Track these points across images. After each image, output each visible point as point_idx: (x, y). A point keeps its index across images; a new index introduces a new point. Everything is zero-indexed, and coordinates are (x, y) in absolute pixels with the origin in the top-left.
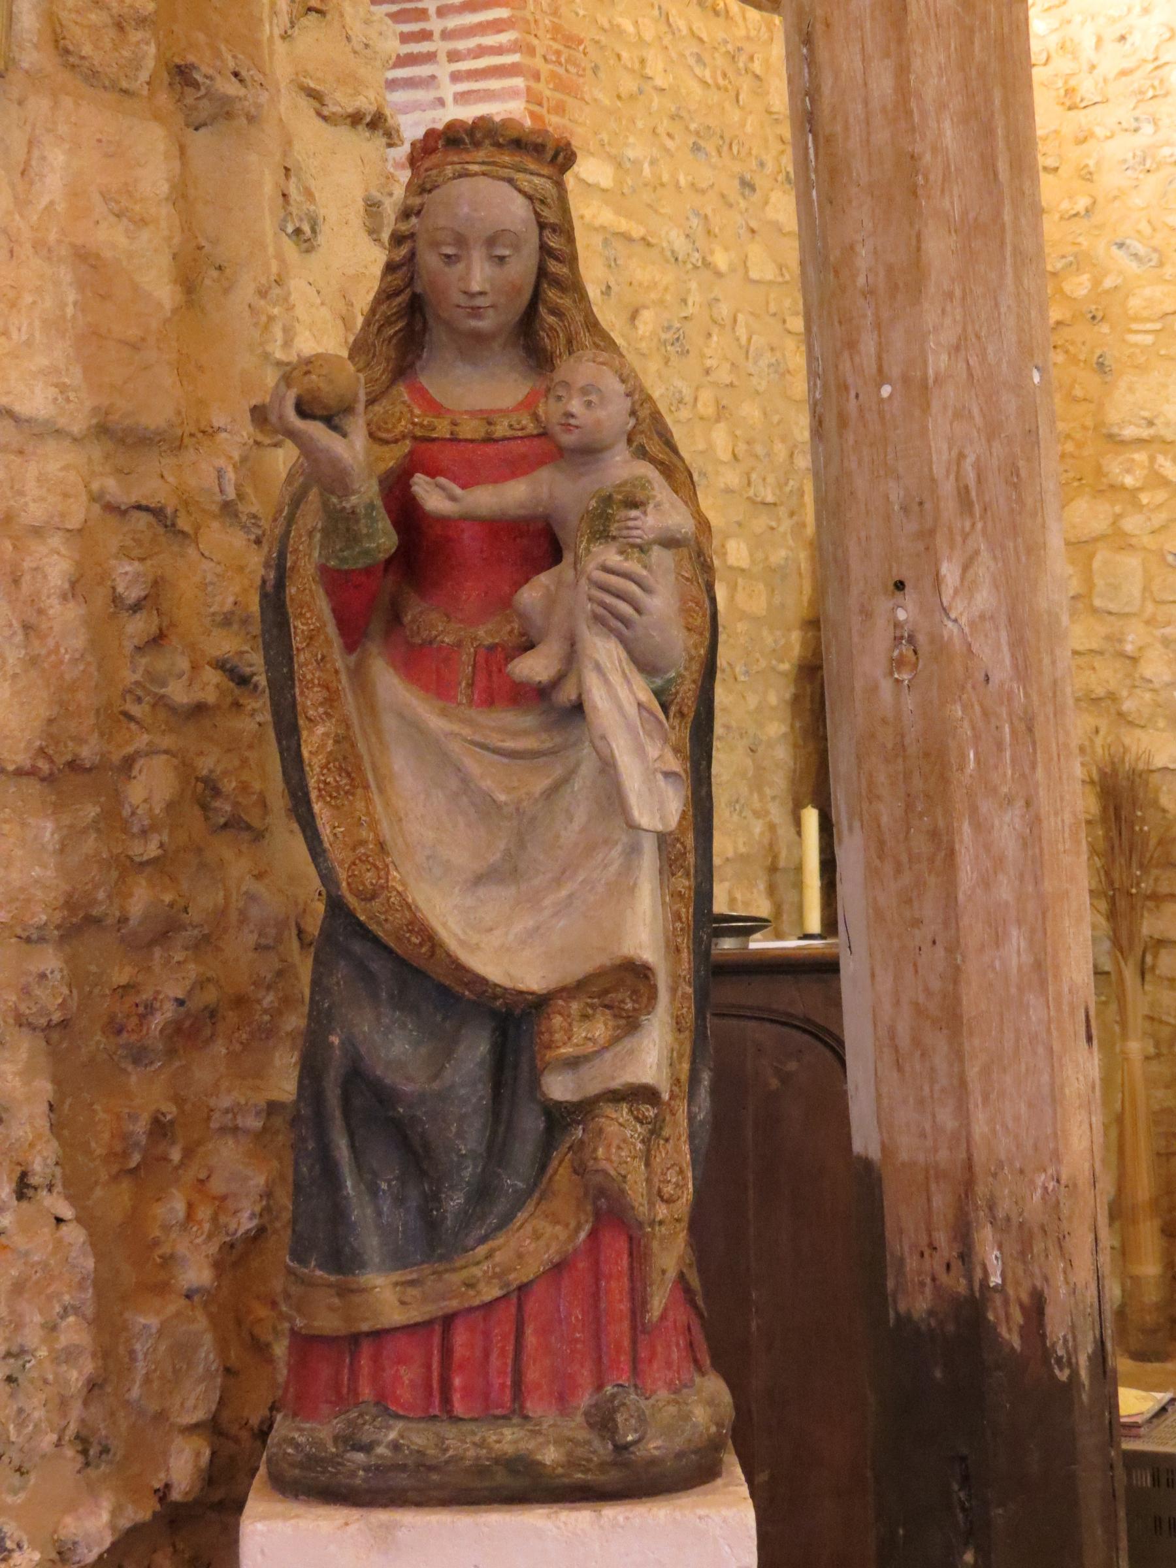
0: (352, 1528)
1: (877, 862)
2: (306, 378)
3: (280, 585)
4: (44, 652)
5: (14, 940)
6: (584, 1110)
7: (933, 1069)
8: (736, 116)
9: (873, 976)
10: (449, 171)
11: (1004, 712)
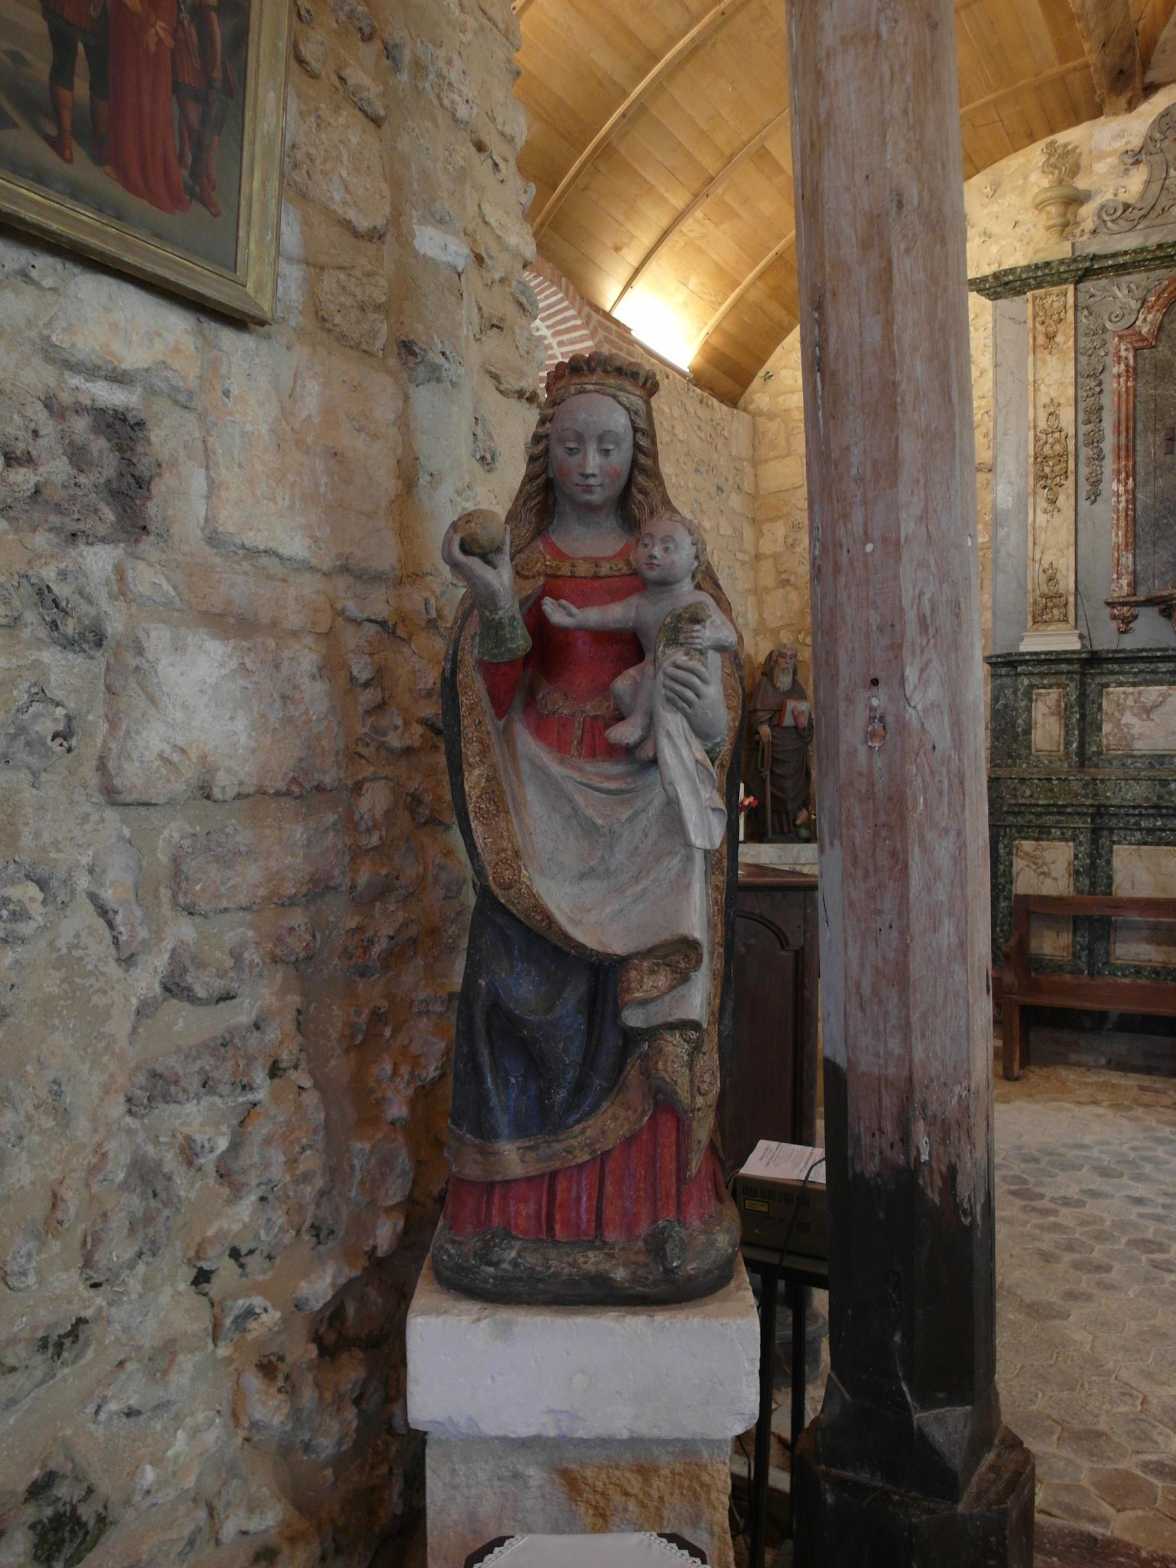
0: (484, 1323)
1: (852, 870)
2: (467, 526)
3: (454, 673)
4: (297, 714)
5: (272, 906)
6: (652, 1033)
7: (887, 1013)
8: (715, 457)
9: (846, 945)
10: (572, 389)
11: (944, 770)
